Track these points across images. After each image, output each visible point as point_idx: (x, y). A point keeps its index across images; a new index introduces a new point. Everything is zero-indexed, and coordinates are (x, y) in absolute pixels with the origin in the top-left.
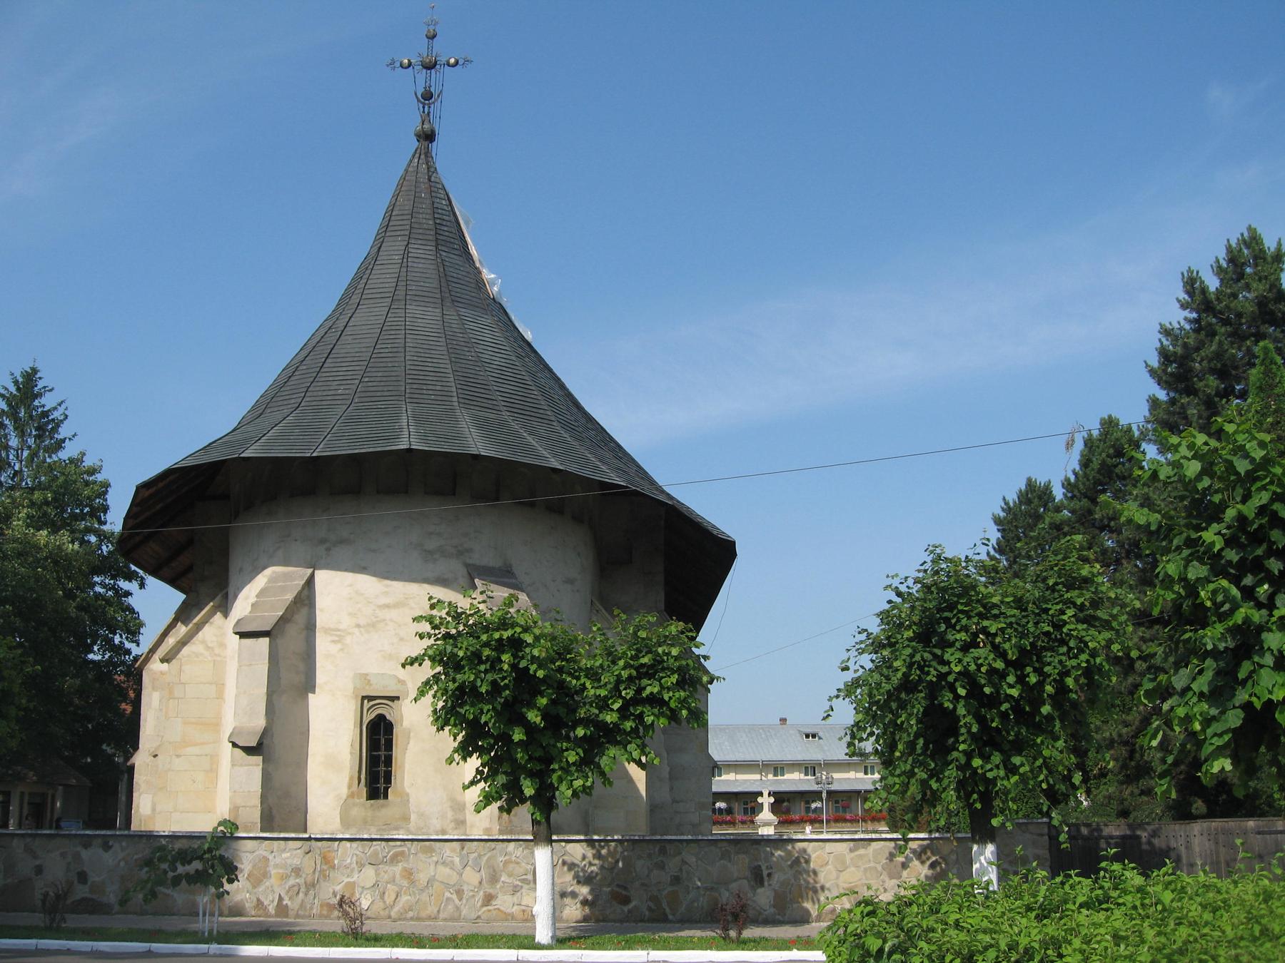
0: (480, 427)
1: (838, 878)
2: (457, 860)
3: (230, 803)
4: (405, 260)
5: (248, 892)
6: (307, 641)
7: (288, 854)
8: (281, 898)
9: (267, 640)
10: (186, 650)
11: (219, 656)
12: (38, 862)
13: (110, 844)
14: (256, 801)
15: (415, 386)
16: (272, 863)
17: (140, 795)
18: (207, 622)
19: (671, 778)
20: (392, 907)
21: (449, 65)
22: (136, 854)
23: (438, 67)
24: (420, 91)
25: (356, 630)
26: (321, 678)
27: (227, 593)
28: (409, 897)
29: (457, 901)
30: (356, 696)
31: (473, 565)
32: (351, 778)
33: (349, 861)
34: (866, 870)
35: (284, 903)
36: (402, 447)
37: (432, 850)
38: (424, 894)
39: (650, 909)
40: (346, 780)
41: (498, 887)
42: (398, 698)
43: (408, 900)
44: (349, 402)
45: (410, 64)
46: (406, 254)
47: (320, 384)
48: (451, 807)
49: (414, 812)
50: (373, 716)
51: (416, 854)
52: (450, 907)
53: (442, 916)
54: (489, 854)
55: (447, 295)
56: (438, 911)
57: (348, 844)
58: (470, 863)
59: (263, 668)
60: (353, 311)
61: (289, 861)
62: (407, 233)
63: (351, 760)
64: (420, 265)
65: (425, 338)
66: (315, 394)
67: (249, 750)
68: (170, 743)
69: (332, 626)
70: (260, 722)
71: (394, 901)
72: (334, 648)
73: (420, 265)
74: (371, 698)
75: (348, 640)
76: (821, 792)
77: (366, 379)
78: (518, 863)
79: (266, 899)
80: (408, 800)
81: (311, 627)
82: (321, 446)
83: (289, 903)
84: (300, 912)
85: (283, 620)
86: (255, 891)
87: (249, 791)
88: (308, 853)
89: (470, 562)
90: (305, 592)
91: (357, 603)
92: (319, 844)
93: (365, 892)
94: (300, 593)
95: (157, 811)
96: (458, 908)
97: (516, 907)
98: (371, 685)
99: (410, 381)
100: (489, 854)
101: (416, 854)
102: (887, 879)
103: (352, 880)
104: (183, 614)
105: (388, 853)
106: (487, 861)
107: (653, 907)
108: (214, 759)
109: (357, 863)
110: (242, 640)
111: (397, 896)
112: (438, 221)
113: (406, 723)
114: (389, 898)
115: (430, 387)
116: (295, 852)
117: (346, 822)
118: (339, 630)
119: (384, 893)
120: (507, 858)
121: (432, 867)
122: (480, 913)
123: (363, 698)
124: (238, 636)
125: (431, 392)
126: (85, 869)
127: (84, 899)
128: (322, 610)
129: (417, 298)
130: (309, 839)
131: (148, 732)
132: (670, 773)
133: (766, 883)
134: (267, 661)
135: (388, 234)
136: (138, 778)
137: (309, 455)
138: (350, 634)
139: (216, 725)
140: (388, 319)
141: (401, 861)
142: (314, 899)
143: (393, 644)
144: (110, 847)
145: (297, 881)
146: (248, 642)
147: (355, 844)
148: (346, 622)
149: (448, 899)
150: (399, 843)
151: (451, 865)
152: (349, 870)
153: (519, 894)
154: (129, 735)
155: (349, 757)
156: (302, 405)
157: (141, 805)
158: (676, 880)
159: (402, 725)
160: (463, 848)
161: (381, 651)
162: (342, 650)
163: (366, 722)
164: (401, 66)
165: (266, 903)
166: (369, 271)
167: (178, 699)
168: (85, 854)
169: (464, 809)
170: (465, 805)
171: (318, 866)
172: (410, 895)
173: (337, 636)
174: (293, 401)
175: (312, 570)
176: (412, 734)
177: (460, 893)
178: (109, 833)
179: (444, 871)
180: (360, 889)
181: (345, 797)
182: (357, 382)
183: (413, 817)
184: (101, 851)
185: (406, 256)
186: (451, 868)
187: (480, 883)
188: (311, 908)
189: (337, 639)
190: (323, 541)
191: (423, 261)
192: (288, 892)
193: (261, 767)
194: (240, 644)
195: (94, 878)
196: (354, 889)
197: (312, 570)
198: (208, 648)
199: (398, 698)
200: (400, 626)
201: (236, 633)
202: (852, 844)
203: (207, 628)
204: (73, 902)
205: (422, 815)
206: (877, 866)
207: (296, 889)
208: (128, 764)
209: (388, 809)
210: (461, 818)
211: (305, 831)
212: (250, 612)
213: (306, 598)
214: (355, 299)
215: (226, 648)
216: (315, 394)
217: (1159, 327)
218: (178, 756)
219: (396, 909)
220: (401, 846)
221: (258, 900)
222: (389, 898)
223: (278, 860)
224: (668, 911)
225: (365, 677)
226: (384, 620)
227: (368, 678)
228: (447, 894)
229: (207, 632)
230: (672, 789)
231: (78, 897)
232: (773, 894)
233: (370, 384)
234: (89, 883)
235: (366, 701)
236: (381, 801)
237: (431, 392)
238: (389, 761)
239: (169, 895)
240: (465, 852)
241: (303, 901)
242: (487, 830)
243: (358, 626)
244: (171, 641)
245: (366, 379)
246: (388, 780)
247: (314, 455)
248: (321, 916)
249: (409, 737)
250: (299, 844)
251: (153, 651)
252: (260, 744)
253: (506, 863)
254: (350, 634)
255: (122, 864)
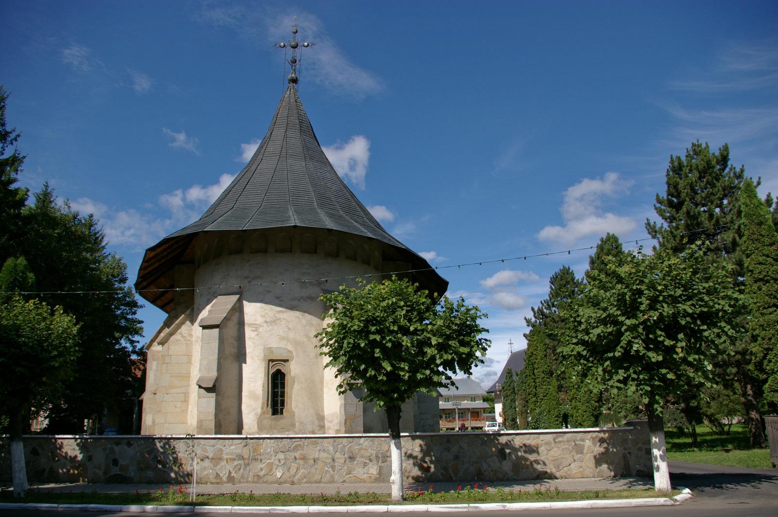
0: (330, 217)
1: (547, 454)
2: (331, 448)
3: (198, 418)
4: (285, 138)
5: (211, 469)
6: (239, 331)
7: (234, 447)
8: (230, 472)
9: (218, 330)
10: (172, 338)
11: (189, 341)
12: (90, 454)
13: (131, 443)
14: (212, 417)
15: (294, 197)
16: (225, 452)
17: (146, 415)
18: (166, 342)
19: (418, 402)
20: (294, 476)
21: (304, 46)
22: (146, 448)
23: (298, 47)
24: (290, 59)
25: (265, 324)
26: (248, 350)
27: (193, 308)
28: (304, 470)
29: (332, 472)
30: (265, 360)
31: (326, 290)
32: (263, 404)
33: (269, 450)
34: (563, 449)
35: (232, 475)
36: (292, 225)
37: (317, 443)
38: (313, 468)
39: (442, 474)
40: (260, 405)
41: (355, 463)
42: (287, 361)
43: (304, 472)
44: (260, 205)
45: (284, 46)
46: (285, 137)
47: (246, 192)
48: (317, 418)
49: (297, 421)
50: (274, 370)
51: (308, 445)
52: (328, 475)
53: (323, 481)
54: (349, 445)
55: (308, 155)
56: (321, 478)
57: (269, 441)
58: (339, 450)
59: (215, 345)
60: (259, 163)
61: (234, 451)
62: (286, 125)
63: (263, 394)
64: (293, 141)
65: (297, 175)
66: (241, 201)
67: (209, 390)
68: (163, 387)
69: (252, 322)
70: (214, 374)
71: (296, 473)
72: (253, 334)
73: (293, 141)
74: (273, 361)
75: (261, 329)
76: (455, 409)
77: (269, 194)
78: (366, 450)
79: (222, 473)
80: (294, 415)
81: (241, 324)
82: (247, 225)
83: (235, 475)
84: (241, 480)
85: (226, 319)
86: (215, 468)
87: (208, 412)
88: (245, 446)
89: (325, 288)
90: (238, 305)
91: (265, 310)
92: (252, 441)
93: (278, 468)
94: (235, 305)
95: (156, 423)
96: (332, 476)
97: (365, 475)
98: (273, 353)
99: (291, 195)
100: (349, 445)
101: (308, 445)
102: (575, 454)
103: (271, 461)
104: (167, 324)
105: (292, 445)
106: (349, 448)
107: (444, 473)
108: (186, 395)
109: (274, 451)
110: (204, 330)
111: (297, 470)
112: (301, 121)
113: (292, 374)
114: (293, 471)
115: (302, 198)
116: (237, 446)
117: (261, 428)
118: (256, 325)
119: (290, 468)
120: (360, 447)
121: (317, 453)
122: (345, 479)
123: (269, 361)
124: (201, 328)
125: (302, 200)
126: (117, 457)
127: (116, 475)
128: (246, 314)
129: (291, 156)
130: (246, 438)
131: (150, 382)
132: (418, 399)
133: (507, 458)
134: (218, 341)
135: (275, 126)
136: (145, 406)
137: (241, 229)
138: (262, 326)
139: (188, 376)
140: (278, 166)
141: (299, 450)
142: (249, 472)
143: (285, 332)
144: (131, 445)
145: (240, 462)
146: (207, 331)
147: (272, 441)
148: (260, 320)
149: (327, 471)
150: (298, 440)
151: (328, 452)
152: (269, 456)
153: (367, 467)
154: (140, 385)
155: (262, 392)
156: (235, 206)
157: (147, 420)
158: (457, 457)
159: (290, 375)
160: (335, 442)
161: (278, 335)
162: (257, 335)
163: (271, 373)
164: (280, 47)
165: (221, 475)
166: (266, 144)
167: (167, 363)
168: (117, 449)
169: (324, 420)
170: (324, 417)
171: (251, 454)
172: (305, 469)
173: (255, 327)
174: (229, 205)
175: (235, 298)
176: (296, 380)
177: (333, 467)
178: (136, 436)
179: (323, 455)
180: (276, 466)
181: (260, 414)
182: (264, 195)
183: (297, 424)
184: (126, 447)
185: (285, 137)
186: (328, 453)
187: (345, 461)
188: (248, 478)
189: (254, 329)
190: (246, 278)
191: (294, 139)
192: (234, 468)
193: (215, 398)
194: (202, 332)
195: (122, 462)
196: (272, 466)
197: (235, 298)
198: (183, 337)
199: (287, 361)
200: (288, 322)
201: (200, 326)
202: (554, 435)
203: (183, 327)
204: (110, 476)
205: (302, 423)
206: (570, 447)
207: (239, 466)
208: (140, 399)
209: (284, 420)
210: (322, 424)
211: (240, 433)
212: (208, 315)
213: (238, 309)
214: (260, 157)
215: (192, 337)
216: (241, 201)
217: (724, 144)
218: (167, 394)
219: (297, 477)
220: (299, 441)
221: (217, 473)
222: (293, 471)
223: (228, 450)
224: (452, 475)
225: (270, 350)
226: (280, 319)
227: (272, 350)
228: (326, 468)
229: (184, 329)
230: (419, 408)
231: (112, 474)
232: (512, 464)
233: (270, 196)
234: (119, 465)
235: (271, 363)
236: (279, 416)
237: (302, 200)
238: (283, 395)
239: (165, 471)
240: (336, 444)
241: (243, 473)
242: (338, 431)
243: (266, 322)
244: (162, 335)
245: (269, 194)
246: (283, 404)
247: (244, 229)
248: (254, 482)
249: (294, 381)
250: (240, 441)
251: (153, 341)
252: (214, 386)
253: (360, 449)
254: (262, 326)
255: (138, 454)
